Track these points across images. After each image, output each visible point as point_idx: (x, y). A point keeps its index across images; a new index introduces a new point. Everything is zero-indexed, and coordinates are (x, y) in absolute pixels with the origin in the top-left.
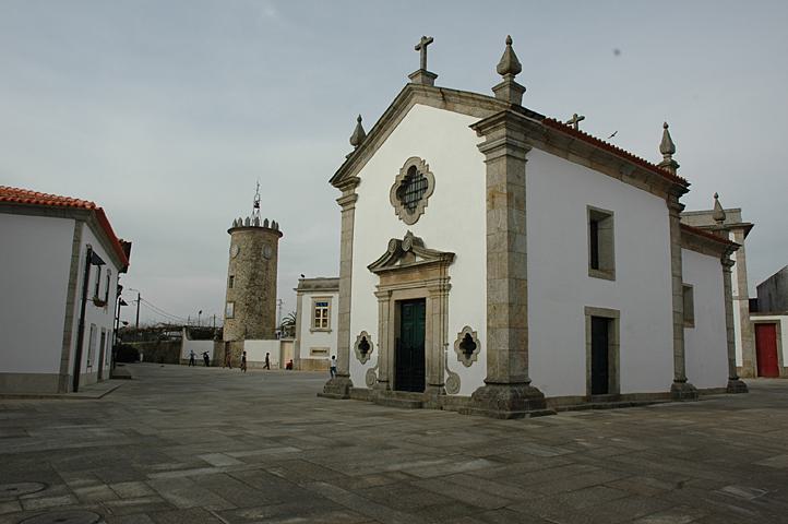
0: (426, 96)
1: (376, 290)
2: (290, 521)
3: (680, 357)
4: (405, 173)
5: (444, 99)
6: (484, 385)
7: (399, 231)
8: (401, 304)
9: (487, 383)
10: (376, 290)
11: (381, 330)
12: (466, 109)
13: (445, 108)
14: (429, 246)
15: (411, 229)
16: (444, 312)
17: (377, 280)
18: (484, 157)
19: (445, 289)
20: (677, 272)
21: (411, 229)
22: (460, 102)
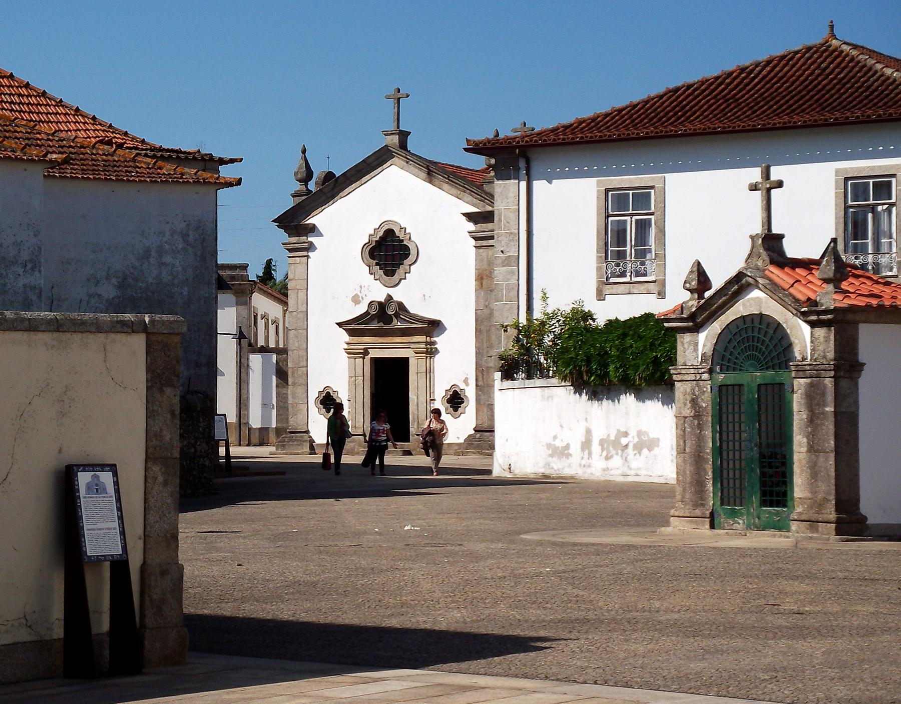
0: (407, 163)
1: (346, 346)
2: (298, 701)
3: (773, 388)
4: (381, 234)
5: (428, 174)
6: (474, 432)
7: (378, 292)
8: (377, 363)
9: (475, 431)
10: (346, 346)
11: (353, 385)
12: (455, 191)
13: (430, 182)
14: (412, 310)
15: (392, 291)
16: (429, 372)
17: (346, 337)
18: (473, 242)
19: (431, 352)
20: (696, 348)
21: (392, 291)
22: (447, 183)
